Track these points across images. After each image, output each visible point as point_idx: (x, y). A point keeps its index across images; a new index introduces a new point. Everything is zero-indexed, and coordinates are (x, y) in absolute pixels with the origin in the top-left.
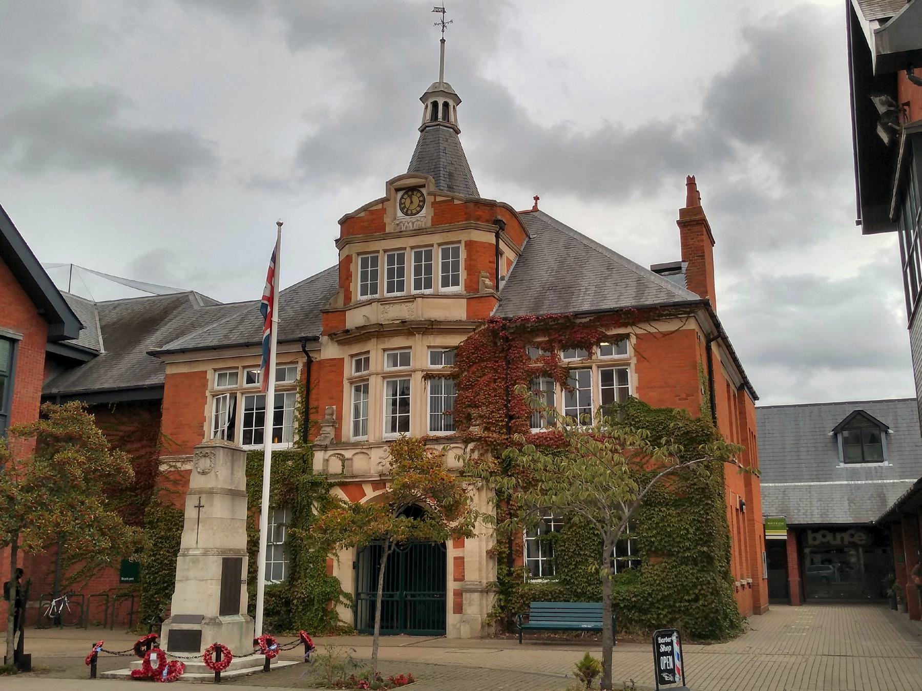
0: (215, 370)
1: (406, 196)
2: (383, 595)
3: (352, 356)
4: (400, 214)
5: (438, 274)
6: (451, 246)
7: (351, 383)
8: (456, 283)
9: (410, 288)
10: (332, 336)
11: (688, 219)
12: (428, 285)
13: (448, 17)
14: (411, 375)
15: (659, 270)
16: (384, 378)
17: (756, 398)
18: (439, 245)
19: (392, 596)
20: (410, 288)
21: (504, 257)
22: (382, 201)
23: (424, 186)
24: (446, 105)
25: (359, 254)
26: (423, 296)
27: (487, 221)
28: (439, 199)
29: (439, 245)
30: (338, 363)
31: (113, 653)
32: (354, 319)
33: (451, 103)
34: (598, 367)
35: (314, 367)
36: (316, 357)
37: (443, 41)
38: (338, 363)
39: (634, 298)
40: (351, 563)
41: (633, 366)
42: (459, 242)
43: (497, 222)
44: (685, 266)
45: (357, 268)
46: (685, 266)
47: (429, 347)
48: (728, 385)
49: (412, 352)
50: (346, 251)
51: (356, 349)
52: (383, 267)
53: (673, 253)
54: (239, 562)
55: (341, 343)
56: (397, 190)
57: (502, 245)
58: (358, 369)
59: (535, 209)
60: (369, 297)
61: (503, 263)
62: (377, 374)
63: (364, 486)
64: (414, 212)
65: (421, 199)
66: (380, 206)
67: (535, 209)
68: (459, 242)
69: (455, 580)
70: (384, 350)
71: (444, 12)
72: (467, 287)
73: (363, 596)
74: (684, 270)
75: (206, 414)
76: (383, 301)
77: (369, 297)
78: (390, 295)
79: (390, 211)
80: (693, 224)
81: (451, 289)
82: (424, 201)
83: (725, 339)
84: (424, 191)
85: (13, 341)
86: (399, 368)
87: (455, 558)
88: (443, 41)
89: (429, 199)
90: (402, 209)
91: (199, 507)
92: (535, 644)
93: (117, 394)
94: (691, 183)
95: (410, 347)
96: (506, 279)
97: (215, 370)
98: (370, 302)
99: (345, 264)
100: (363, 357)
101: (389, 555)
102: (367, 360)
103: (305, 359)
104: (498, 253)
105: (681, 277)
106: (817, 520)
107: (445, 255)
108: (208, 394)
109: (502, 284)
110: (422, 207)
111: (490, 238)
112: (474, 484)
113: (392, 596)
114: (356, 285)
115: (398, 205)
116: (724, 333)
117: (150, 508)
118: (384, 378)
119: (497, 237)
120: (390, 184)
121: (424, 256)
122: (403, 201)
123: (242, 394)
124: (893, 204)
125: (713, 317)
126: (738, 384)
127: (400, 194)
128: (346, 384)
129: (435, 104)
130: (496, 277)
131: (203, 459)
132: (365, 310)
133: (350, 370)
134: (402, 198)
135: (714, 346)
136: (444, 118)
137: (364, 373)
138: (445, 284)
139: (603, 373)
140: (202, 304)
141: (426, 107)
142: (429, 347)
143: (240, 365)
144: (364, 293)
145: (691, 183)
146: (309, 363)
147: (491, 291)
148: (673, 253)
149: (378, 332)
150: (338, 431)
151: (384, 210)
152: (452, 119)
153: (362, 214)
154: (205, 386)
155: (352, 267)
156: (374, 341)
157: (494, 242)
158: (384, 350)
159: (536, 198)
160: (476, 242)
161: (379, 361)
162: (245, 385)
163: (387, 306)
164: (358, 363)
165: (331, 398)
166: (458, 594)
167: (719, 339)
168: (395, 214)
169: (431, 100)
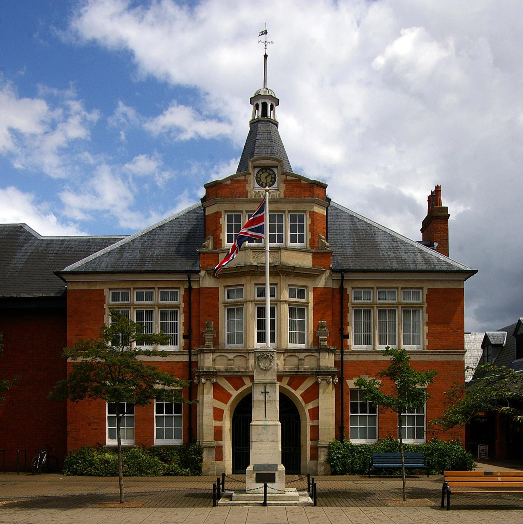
0: (110, 289)
4: (256, 185)
6: (297, 214)
8: (301, 240)
10: (208, 272)
13: (270, 37)
14: (277, 304)
16: (256, 304)
18: (289, 212)
25: (226, 212)
28: (289, 178)
29: (289, 212)
34: (402, 307)
36: (194, 286)
37: (266, 56)
42: (305, 212)
49: (244, 288)
62: (252, 302)
63: (243, 378)
71: (266, 33)
72: (312, 245)
81: (297, 245)
84: (275, 170)
86: (120, 302)
87: (311, 426)
88: (266, 56)
90: (258, 182)
91: (265, 392)
97: (225, 287)
107: (293, 219)
108: (105, 306)
112: (326, 380)
123: (134, 308)
124: (98, 254)
127: (256, 171)
128: (221, 307)
131: (264, 360)
133: (223, 296)
134: (258, 173)
138: (293, 240)
139: (162, 313)
146: (189, 290)
153: (229, 182)
154: (103, 301)
156: (248, 278)
160: (317, 213)
165: (209, 316)
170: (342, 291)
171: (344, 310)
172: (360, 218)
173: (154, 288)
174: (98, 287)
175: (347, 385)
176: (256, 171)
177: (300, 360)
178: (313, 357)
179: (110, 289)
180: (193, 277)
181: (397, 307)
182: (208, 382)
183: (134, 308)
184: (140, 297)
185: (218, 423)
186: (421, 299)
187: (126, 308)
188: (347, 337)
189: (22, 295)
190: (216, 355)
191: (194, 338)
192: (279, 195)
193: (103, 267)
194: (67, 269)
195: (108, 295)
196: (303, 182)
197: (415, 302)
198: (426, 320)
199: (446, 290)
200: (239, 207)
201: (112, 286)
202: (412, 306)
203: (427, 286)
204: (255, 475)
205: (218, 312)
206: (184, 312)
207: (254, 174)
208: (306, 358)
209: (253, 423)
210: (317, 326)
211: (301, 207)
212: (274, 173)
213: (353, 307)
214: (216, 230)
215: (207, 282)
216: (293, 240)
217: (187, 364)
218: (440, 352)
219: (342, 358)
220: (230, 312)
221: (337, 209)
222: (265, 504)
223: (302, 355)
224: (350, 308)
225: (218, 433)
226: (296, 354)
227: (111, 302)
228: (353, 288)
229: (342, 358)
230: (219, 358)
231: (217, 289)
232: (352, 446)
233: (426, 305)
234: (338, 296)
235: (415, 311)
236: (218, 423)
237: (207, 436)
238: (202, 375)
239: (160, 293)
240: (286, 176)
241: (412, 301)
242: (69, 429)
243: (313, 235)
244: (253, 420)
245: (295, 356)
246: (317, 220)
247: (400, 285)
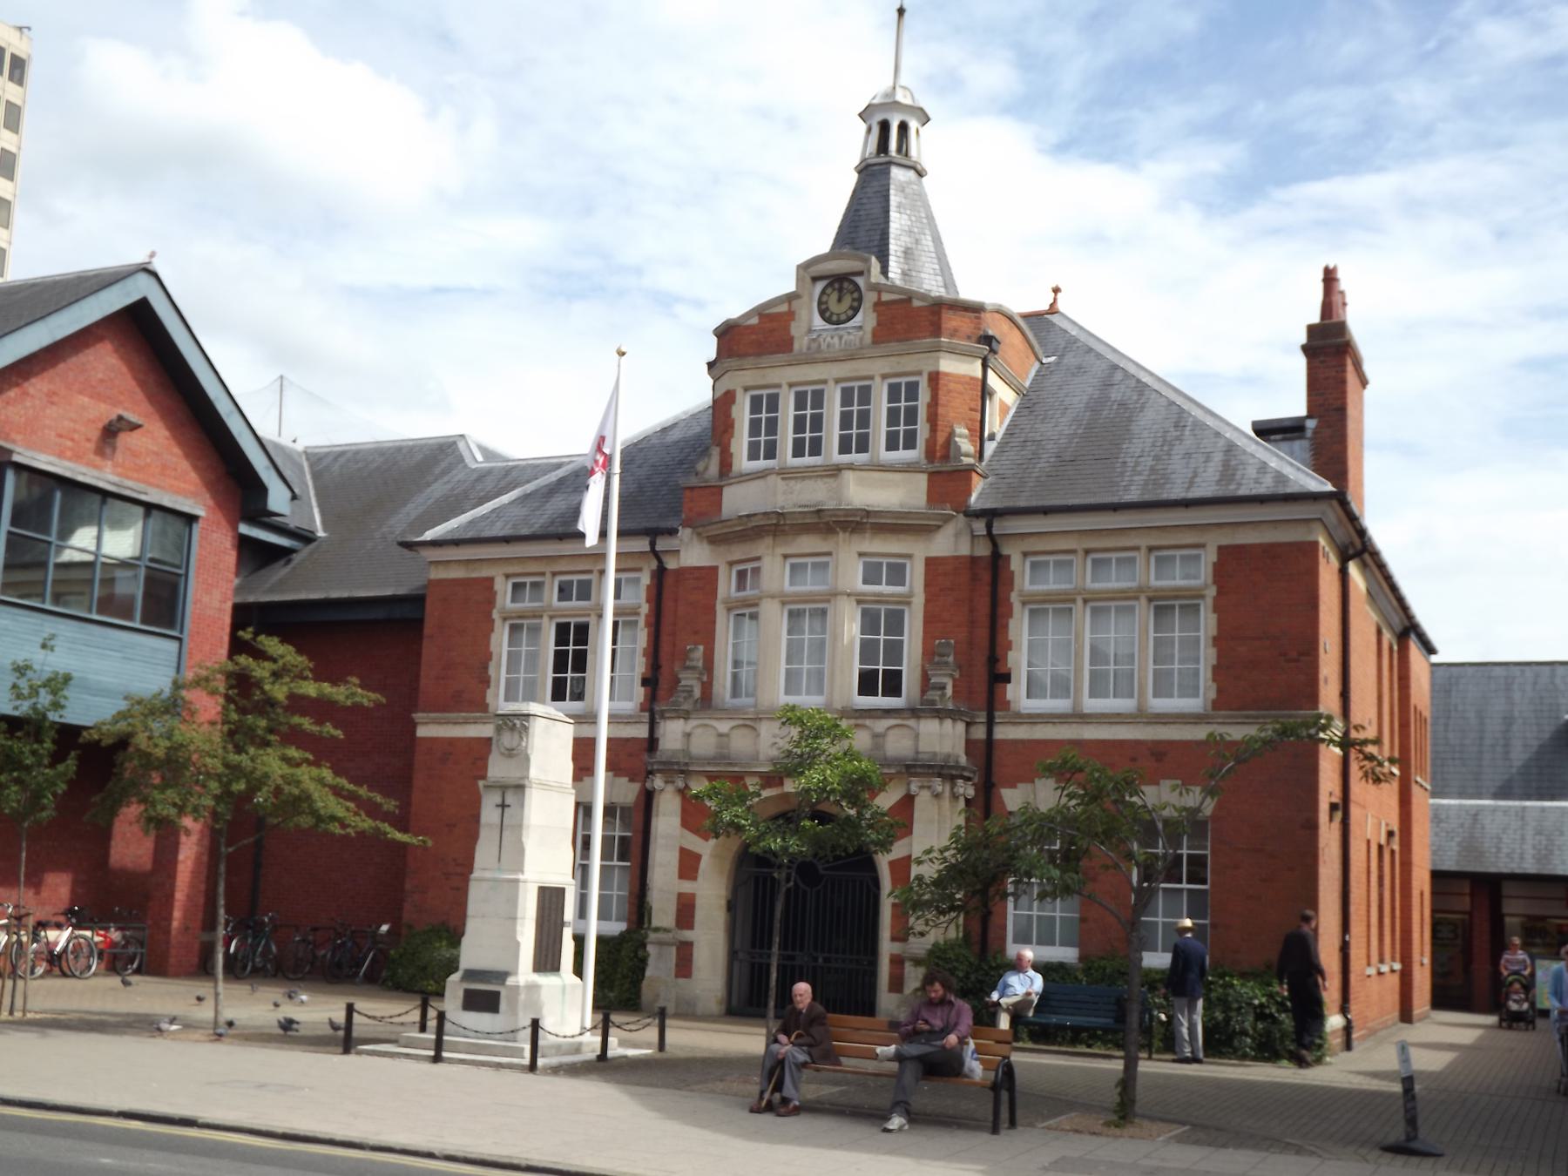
0: (507, 576)
1: (829, 291)
2: (769, 956)
3: (731, 564)
4: (818, 322)
5: (880, 428)
7: (729, 610)
8: (910, 443)
9: (832, 453)
11: (1320, 343)
12: (863, 446)
15: (1265, 431)
17: (1430, 649)
18: (837, 381)
19: (792, 958)
20: (832, 453)
21: (996, 398)
22: (790, 298)
23: (860, 273)
24: (903, 127)
25: (746, 389)
26: (851, 467)
27: (969, 338)
28: (886, 297)
30: (707, 576)
31: (374, 1018)
32: (738, 501)
33: (913, 124)
35: (669, 581)
36: (671, 564)
38: (707, 576)
39: (1218, 482)
40: (723, 902)
41: (1209, 601)
42: (919, 373)
43: (988, 340)
44: (1311, 424)
45: (742, 414)
46: (1311, 424)
47: (861, 555)
48: (1379, 632)
50: (727, 383)
51: (738, 552)
52: (788, 412)
53: (1292, 403)
54: (559, 893)
55: (714, 541)
56: (815, 279)
57: (993, 380)
58: (741, 585)
59: (1053, 310)
60: (762, 464)
61: (992, 410)
62: (849, 595)
64: (843, 317)
65: (856, 295)
66: (784, 308)
67: (1053, 310)
68: (919, 373)
69: (894, 939)
70: (786, 557)
72: (930, 453)
73: (741, 955)
74: (1309, 433)
75: (493, 647)
76: (786, 474)
77: (762, 464)
78: (799, 461)
79: (802, 314)
80: (1329, 350)
81: (902, 455)
82: (860, 300)
83: (1375, 555)
84: (860, 281)
85: (191, 519)
89: (870, 298)
90: (822, 313)
91: (503, 806)
92: (674, 425)
93: (368, 622)
94: (1330, 278)
95: (829, 554)
96: (999, 437)
98: (761, 475)
99: (722, 405)
100: (749, 566)
101: (788, 890)
102: (756, 571)
103: (654, 564)
104: (985, 392)
105: (1301, 446)
106: (1530, 867)
108: (495, 615)
109: (990, 448)
110: (856, 310)
111: (975, 369)
113: (792, 958)
114: (741, 441)
115: (815, 305)
116: (1372, 545)
117: (436, 809)
118: (784, 603)
119: (985, 366)
120: (804, 268)
121: (855, 395)
122: (825, 298)
125: (1353, 519)
126: (1398, 628)
127: (820, 286)
128: (720, 609)
129: (885, 126)
130: (980, 436)
132: (754, 487)
133: (726, 586)
135: (1353, 569)
136: (899, 150)
137: (748, 593)
138: (892, 445)
140: (479, 458)
141: (869, 130)
142: (861, 555)
143: (548, 569)
144: (753, 455)
145: (1330, 278)
146: (660, 574)
147: (971, 461)
148: (1292, 403)
149: (776, 526)
150: (707, 688)
151: (791, 315)
152: (913, 152)
153: (754, 321)
154: (490, 600)
155: (735, 411)
156: (769, 540)
157: (979, 374)
158: (786, 557)
159: (1056, 290)
160: (947, 374)
161: (775, 572)
162: (555, 602)
163: (792, 483)
164: (742, 575)
165: (696, 633)
166: (897, 962)
167: (1366, 556)
168: (811, 320)
169: (879, 117)
170: (997, 562)
171: (653, 620)
172: (1132, 370)
173: (543, 574)
174: (484, 572)
175: (1002, 803)
176: (820, 286)
177: (875, 736)
178: (905, 731)
179: (507, 576)
180: (661, 545)
181: (1137, 598)
182: (670, 788)
183: (551, 617)
184: (564, 592)
185: (687, 887)
186: (1199, 574)
187: (535, 617)
188: (1007, 678)
189: (335, 594)
190: (693, 723)
191: (664, 684)
192: (861, 339)
193: (497, 530)
194: (429, 535)
195: (503, 589)
196: (916, 303)
197: (1063, 586)
198: (1213, 631)
199: (1270, 550)
200: (774, 376)
201: (557, 568)
202: (1177, 594)
203: (1214, 541)
204: (461, 994)
205: (714, 622)
206: (648, 624)
207: (811, 295)
208: (891, 732)
209: (476, 874)
210: (929, 654)
211: (909, 363)
212: (856, 285)
213: (1024, 604)
214: (725, 431)
215: (692, 553)
216: (892, 445)
217: (646, 745)
218: (1247, 717)
219: (990, 732)
220: (515, 629)
221: (1091, 350)
222: (437, 1059)
223: (881, 725)
224: (1017, 607)
225: (686, 911)
226: (868, 722)
227: (509, 604)
228: (1025, 554)
229: (990, 732)
230: (699, 731)
231: (714, 569)
232: (1150, 971)
233: (1212, 592)
234: (986, 576)
235: (1166, 607)
236: (687, 887)
237: (663, 913)
238: (659, 771)
239: (1089, 563)
240: (879, 293)
241: (1179, 582)
242: (408, 886)
243: (934, 428)
244: (476, 865)
245: (864, 726)
246: (949, 391)
247: (1144, 541)
